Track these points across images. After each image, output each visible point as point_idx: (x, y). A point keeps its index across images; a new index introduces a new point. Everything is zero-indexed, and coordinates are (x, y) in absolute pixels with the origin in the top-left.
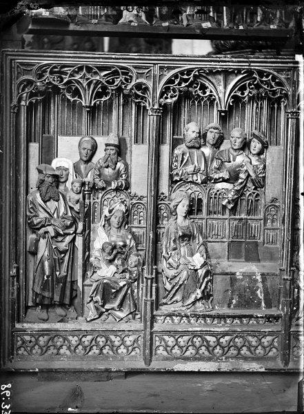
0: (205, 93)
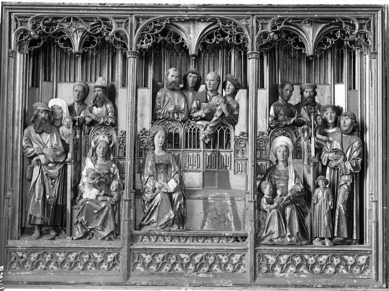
0: (177, 41)
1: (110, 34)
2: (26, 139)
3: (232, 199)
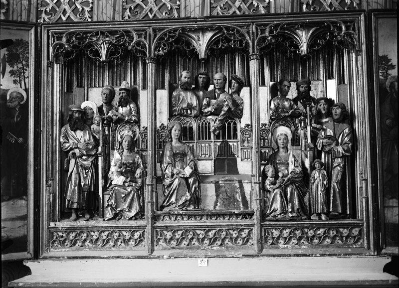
2: (64, 136)
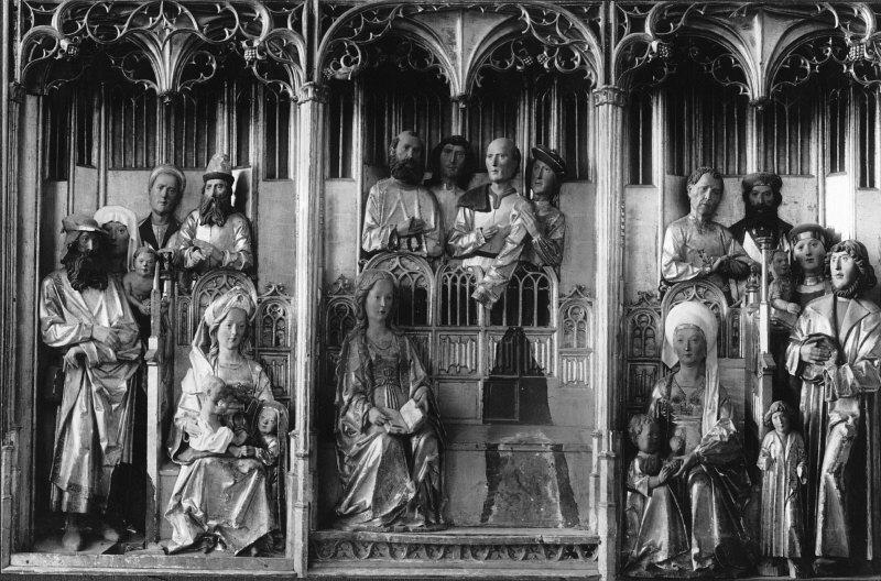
1: (256, 44)
2: (48, 305)
3: (557, 449)
